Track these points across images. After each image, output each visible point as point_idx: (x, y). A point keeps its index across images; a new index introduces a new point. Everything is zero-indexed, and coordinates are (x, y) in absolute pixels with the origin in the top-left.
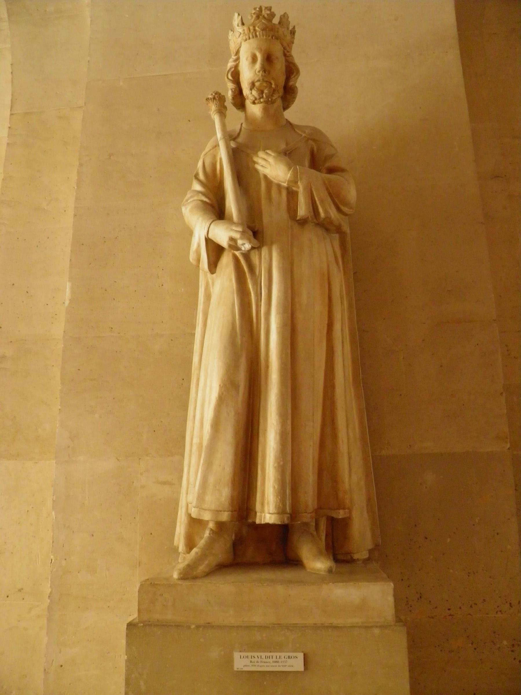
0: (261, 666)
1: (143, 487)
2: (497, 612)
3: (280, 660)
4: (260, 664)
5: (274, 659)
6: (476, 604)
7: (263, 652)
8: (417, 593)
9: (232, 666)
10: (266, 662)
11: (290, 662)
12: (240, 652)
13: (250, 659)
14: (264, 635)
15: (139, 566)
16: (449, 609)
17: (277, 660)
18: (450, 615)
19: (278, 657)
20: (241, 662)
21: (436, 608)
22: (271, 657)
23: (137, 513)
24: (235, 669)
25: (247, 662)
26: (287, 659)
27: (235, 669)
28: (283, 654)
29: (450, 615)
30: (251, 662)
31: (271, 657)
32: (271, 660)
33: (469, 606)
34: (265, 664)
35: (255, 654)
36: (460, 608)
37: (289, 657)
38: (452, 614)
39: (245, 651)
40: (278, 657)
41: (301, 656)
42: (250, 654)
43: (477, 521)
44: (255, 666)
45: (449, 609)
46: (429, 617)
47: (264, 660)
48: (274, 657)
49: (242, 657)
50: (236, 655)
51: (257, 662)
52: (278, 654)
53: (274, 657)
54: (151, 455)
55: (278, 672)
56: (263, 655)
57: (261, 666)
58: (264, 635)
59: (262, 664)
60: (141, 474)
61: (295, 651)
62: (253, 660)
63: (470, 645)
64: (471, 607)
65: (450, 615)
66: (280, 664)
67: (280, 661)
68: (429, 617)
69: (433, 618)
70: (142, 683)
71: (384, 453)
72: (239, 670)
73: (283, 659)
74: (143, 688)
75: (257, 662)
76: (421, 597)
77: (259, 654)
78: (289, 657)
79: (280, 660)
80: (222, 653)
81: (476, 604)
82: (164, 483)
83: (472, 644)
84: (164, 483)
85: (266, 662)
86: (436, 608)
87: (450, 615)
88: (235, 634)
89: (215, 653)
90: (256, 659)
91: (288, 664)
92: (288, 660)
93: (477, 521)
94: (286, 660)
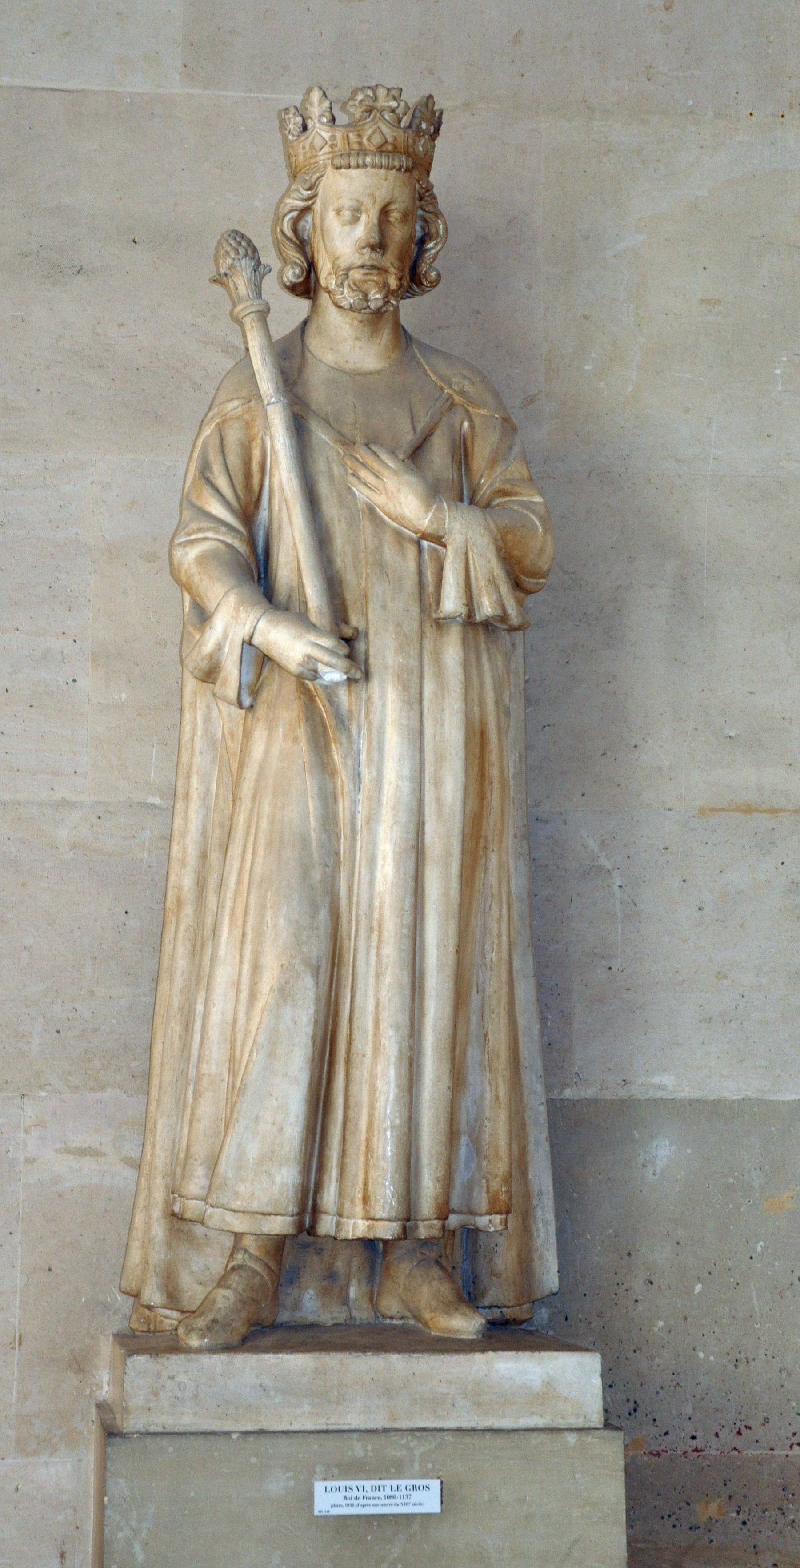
0: (363, 1506)
1: (30, 1161)
2: (791, 1447)
3: (397, 1494)
4: (362, 1502)
5: (388, 1492)
6: (750, 1428)
7: (369, 1478)
8: (628, 1400)
9: (311, 1507)
10: (374, 1498)
11: (416, 1496)
12: (325, 1479)
13: (343, 1493)
14: (369, 1448)
15: (20, 1344)
16: (694, 1438)
17: (393, 1493)
18: (693, 1451)
19: (395, 1488)
20: (330, 1498)
21: (666, 1434)
22: (381, 1489)
23: (17, 1221)
24: (316, 1513)
25: (338, 1498)
26: (412, 1492)
27: (316, 1513)
28: (403, 1483)
29: (696, 1450)
30: (345, 1498)
31: (381, 1489)
32: (381, 1494)
33: (735, 1431)
34: (372, 1502)
35: (353, 1483)
36: (717, 1435)
37: (414, 1488)
38: (699, 1448)
39: (333, 1478)
40: (395, 1488)
41: (435, 1484)
42: (342, 1484)
43: (759, 1249)
44: (352, 1505)
45: (694, 1438)
46: (651, 1453)
47: (370, 1494)
48: (388, 1489)
49: (329, 1489)
50: (319, 1487)
51: (357, 1498)
52: (395, 1483)
53: (388, 1489)
54: (48, 1088)
55: (394, 1515)
56: (368, 1484)
57: (363, 1506)
58: (369, 1448)
59: (365, 1502)
60: (27, 1131)
61: (425, 1475)
62: (348, 1495)
63: (734, 1515)
64: (739, 1433)
65: (696, 1450)
66: (398, 1501)
67: (398, 1496)
68: (651, 1453)
69: (658, 1455)
70: (137, 1549)
71: (568, 1093)
72: (324, 1514)
73: (404, 1492)
74: (140, 1556)
75: (357, 1498)
76: (635, 1410)
77: (360, 1483)
78: (414, 1488)
79: (397, 1494)
80: (292, 1483)
81: (750, 1428)
82: (82, 1152)
83: (738, 1512)
84: (82, 1152)
85: (374, 1498)
86: (666, 1434)
87: (693, 1451)
88: (316, 1447)
89: (277, 1484)
90: (355, 1493)
91: (412, 1501)
92: (414, 1493)
93: (759, 1249)
94: (408, 1493)
